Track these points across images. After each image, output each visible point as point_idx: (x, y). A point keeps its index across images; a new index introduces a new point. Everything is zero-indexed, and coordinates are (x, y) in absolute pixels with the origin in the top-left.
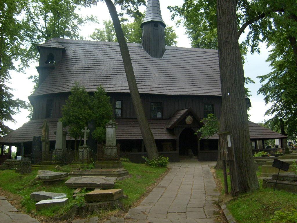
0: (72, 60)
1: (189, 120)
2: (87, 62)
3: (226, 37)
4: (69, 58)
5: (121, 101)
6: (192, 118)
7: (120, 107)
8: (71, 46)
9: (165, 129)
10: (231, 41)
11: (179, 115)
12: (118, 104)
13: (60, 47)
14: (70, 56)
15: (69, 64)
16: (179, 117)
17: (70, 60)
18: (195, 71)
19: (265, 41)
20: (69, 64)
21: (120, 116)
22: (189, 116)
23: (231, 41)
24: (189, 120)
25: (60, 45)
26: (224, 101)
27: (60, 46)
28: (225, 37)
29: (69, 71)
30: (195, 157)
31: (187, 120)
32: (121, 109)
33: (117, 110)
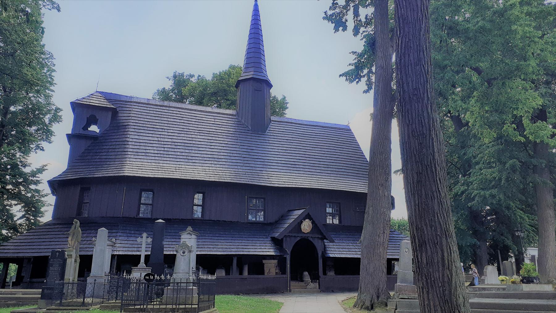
0: (127, 127)
1: (306, 226)
2: (157, 133)
3: (415, 87)
4: (121, 124)
5: (203, 193)
6: (310, 224)
7: (200, 203)
8: (127, 106)
9: (269, 239)
10: (423, 94)
11: (292, 217)
12: (198, 198)
13: (109, 106)
14: (123, 121)
15: (122, 133)
16: (291, 221)
17: (124, 127)
18: (172, 120)
19: (37, 179)
20: (122, 133)
21: (200, 216)
22: (307, 220)
23: (423, 94)
24: (306, 226)
25: (108, 103)
26: (369, 202)
27: (109, 105)
28: (413, 86)
29: (121, 143)
30: (312, 285)
31: (302, 226)
32: (203, 206)
33: (195, 207)
